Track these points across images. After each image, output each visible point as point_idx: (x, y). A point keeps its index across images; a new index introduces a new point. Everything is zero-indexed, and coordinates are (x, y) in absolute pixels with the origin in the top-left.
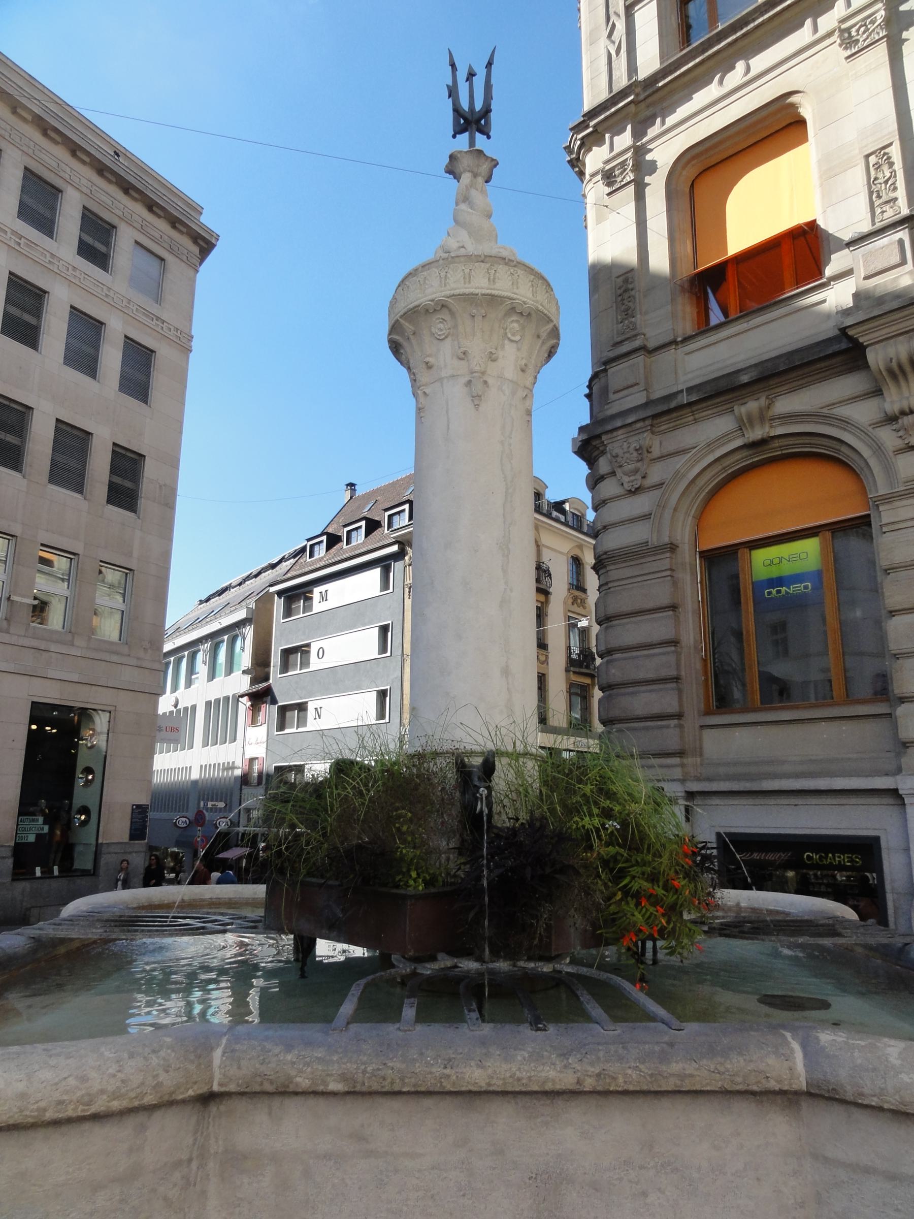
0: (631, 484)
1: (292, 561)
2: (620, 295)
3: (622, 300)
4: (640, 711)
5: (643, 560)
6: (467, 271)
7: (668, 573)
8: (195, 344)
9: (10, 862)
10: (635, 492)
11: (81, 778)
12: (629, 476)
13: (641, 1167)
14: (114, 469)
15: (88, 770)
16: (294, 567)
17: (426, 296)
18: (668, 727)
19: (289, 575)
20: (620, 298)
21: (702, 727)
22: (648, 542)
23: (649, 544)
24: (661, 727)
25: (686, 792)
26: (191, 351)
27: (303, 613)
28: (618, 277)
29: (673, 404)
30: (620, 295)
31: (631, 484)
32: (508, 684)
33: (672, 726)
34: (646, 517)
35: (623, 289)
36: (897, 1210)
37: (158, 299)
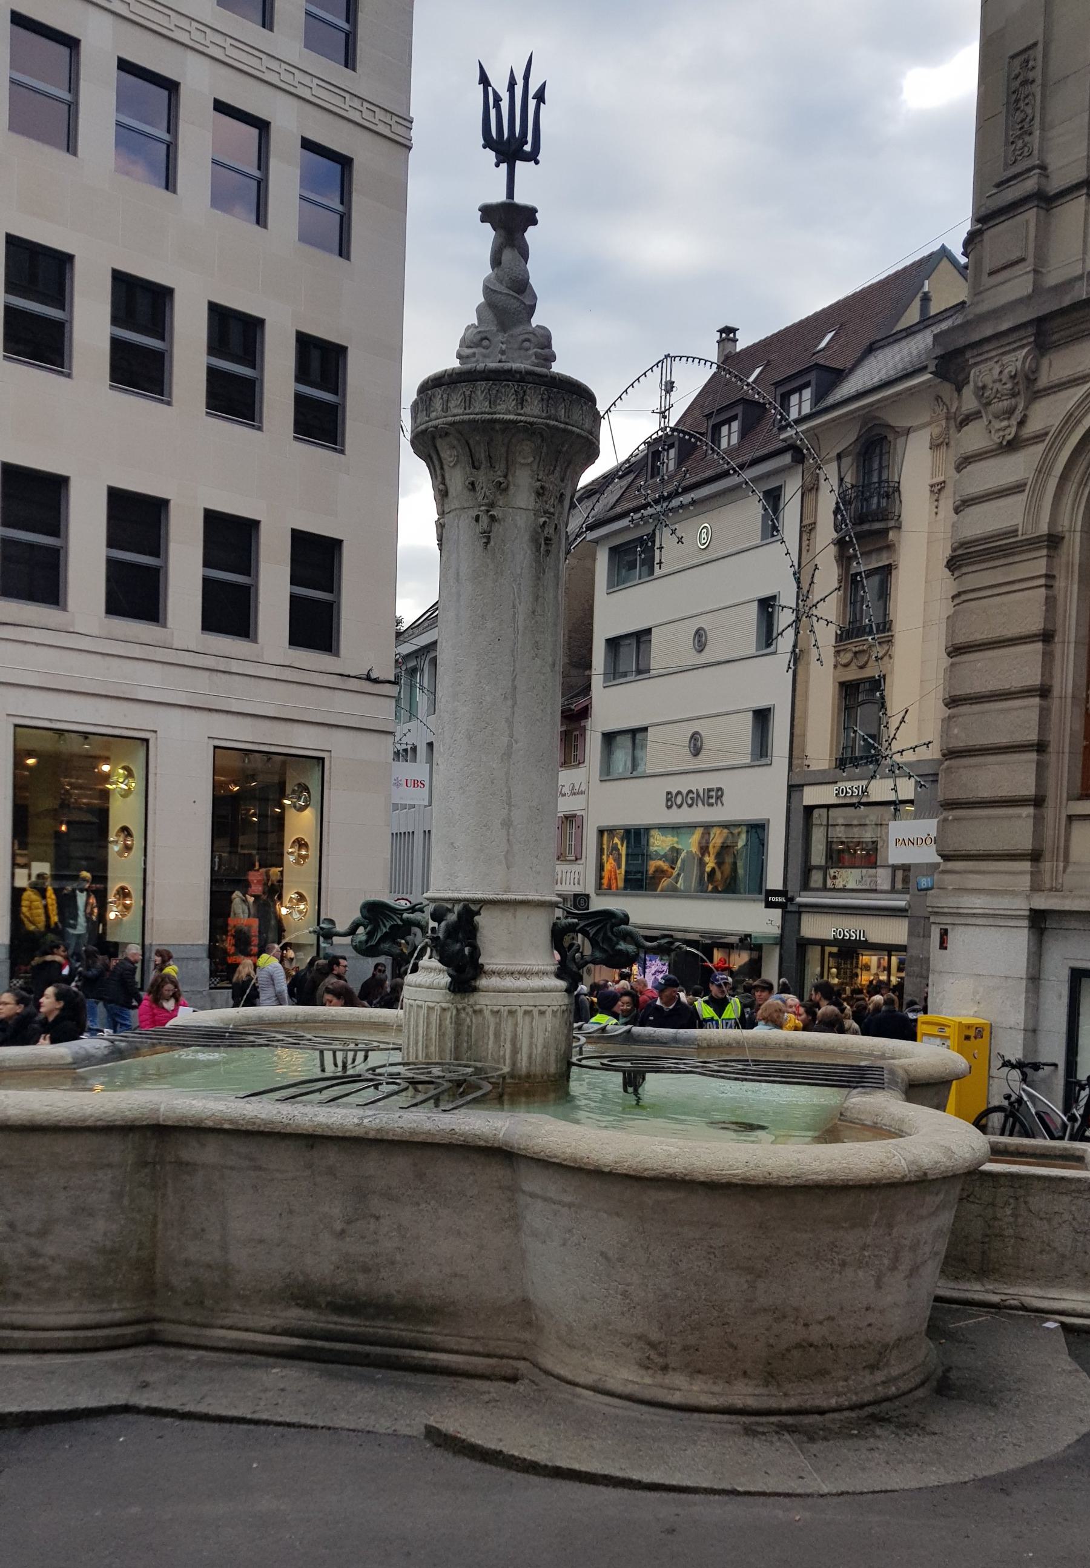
0: (1001, 433)
1: (625, 482)
2: (1014, 92)
3: (1017, 101)
4: (986, 793)
5: (1010, 560)
6: (468, 393)
7: (1042, 581)
8: (416, 134)
9: (205, 965)
10: (1012, 446)
11: (292, 853)
12: (1002, 421)
13: (415, 1189)
14: (302, 374)
15: (300, 843)
16: (627, 495)
17: (430, 421)
18: (1019, 816)
19: (618, 510)
20: (1014, 97)
21: (1070, 818)
22: (1017, 531)
23: (1020, 533)
24: (1010, 817)
25: (1031, 910)
26: (410, 148)
27: (640, 579)
28: (1013, 57)
29: (1067, 301)
30: (1014, 92)
31: (1001, 433)
32: (508, 835)
33: (1024, 816)
34: (1017, 488)
35: (1019, 81)
36: (547, 1219)
37: (349, 61)
